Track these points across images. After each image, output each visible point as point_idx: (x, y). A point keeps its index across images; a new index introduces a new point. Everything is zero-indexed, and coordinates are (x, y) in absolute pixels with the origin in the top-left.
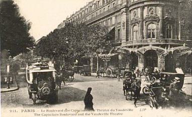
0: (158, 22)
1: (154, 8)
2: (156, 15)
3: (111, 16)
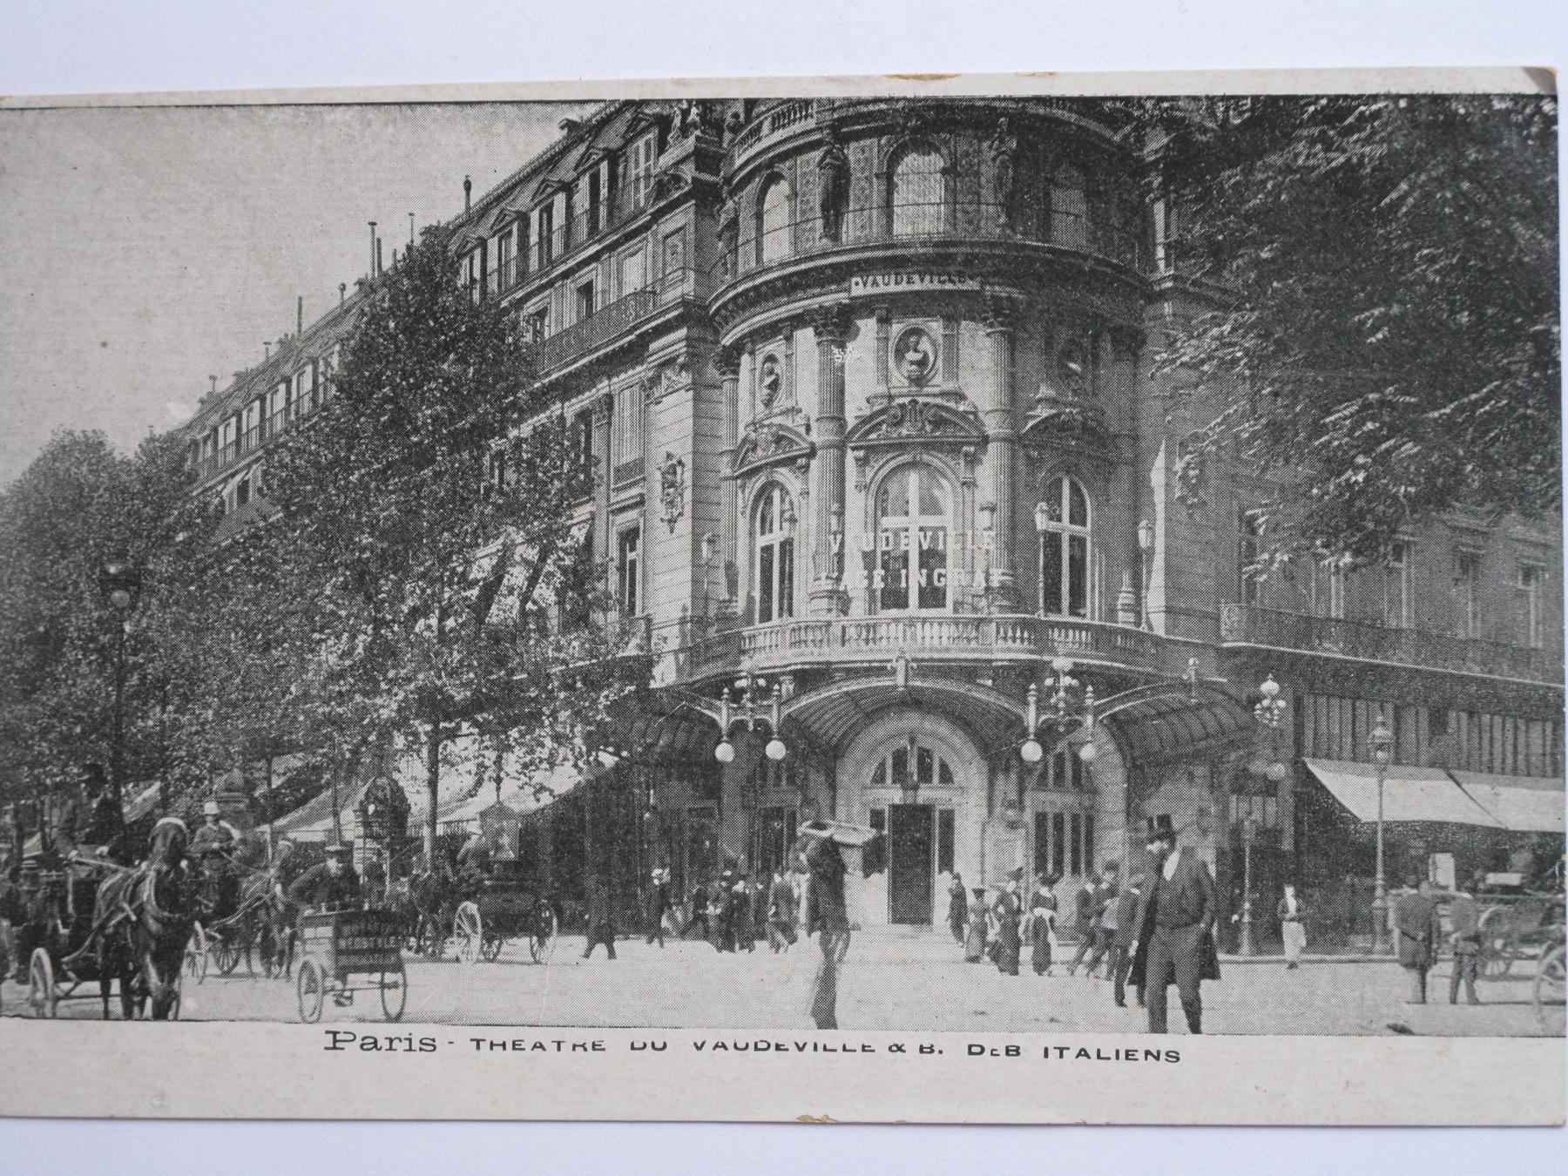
0: (973, 461)
1: (936, 327)
2: (959, 396)
3: (603, 387)
